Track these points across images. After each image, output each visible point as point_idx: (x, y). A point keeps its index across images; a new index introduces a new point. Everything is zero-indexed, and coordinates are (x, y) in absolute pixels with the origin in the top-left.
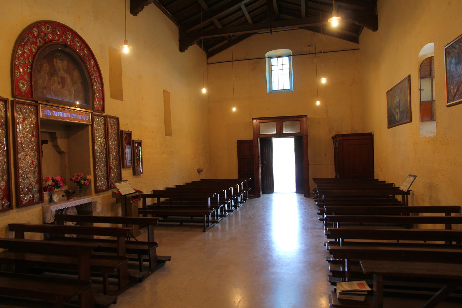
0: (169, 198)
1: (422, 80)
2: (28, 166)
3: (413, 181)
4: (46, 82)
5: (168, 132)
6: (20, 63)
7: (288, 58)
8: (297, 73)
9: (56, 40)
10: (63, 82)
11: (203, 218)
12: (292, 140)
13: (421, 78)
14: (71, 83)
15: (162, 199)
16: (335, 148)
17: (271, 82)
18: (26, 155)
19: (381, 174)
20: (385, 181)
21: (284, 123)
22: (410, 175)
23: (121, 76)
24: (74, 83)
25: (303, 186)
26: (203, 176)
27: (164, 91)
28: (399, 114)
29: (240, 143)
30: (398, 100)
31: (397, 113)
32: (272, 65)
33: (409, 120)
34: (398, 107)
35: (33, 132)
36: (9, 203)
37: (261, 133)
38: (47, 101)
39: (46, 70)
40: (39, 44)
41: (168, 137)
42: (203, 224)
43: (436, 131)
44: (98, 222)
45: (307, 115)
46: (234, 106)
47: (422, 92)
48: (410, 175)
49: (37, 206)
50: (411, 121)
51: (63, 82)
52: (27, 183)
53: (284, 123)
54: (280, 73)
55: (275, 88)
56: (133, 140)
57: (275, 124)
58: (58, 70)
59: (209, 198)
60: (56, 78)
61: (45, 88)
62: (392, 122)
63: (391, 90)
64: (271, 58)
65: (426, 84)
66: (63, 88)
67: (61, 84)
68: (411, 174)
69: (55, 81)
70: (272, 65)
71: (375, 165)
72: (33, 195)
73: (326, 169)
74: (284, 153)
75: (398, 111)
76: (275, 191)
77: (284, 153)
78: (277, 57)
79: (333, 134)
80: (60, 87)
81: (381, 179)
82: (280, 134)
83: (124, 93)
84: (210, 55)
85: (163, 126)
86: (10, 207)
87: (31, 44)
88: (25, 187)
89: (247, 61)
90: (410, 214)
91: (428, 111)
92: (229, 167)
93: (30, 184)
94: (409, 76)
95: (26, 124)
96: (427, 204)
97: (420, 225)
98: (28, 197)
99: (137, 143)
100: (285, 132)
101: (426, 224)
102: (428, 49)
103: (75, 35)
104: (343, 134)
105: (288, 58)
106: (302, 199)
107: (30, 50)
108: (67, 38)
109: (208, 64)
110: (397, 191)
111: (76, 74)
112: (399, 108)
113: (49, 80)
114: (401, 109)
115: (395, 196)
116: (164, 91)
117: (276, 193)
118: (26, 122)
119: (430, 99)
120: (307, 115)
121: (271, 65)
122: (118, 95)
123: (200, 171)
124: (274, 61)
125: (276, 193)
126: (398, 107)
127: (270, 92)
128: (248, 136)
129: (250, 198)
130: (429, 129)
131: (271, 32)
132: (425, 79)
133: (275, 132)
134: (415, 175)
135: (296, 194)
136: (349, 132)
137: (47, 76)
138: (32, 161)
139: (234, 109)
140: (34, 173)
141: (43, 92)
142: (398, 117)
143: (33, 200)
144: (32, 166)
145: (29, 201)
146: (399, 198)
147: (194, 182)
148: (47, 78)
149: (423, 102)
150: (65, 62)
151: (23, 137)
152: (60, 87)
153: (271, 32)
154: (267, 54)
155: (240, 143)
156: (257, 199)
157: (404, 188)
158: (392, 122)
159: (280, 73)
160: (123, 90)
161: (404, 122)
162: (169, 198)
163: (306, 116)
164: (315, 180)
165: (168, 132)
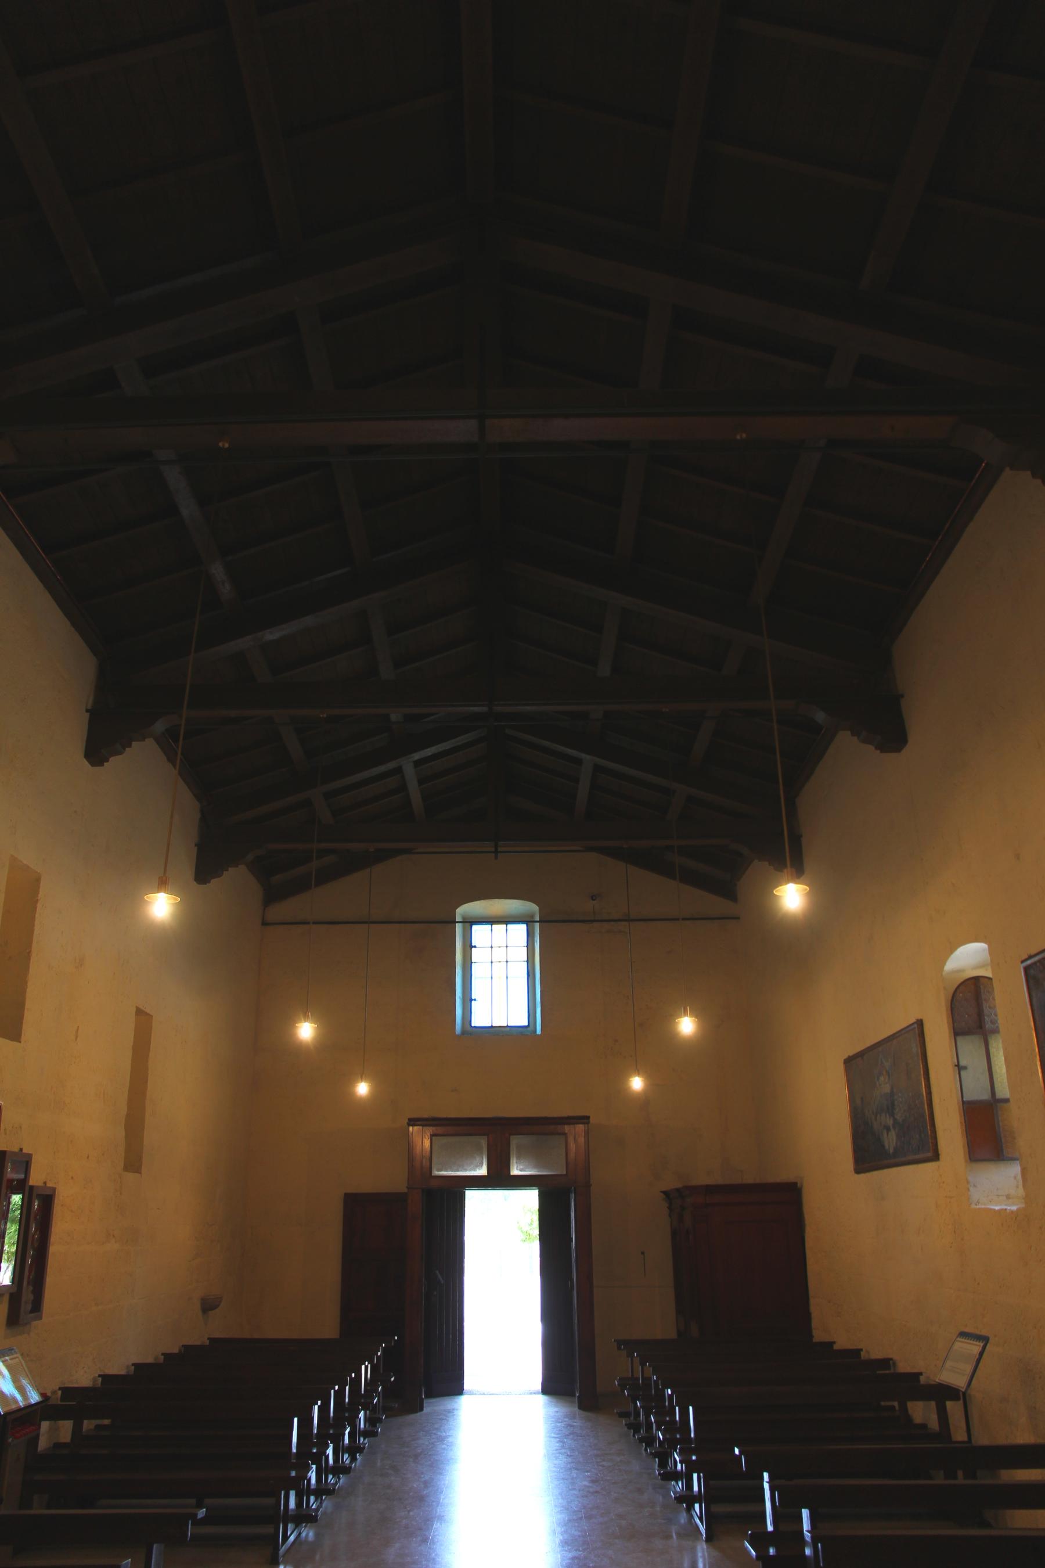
1: (959, 1039)
3: (981, 1354)
5: (133, 1162)
7: (524, 927)
8: (555, 973)
11: (271, 1501)
12: (529, 1199)
13: (958, 1032)
15: (88, 1425)
16: (674, 1233)
17: (468, 1000)
19: (833, 1324)
20: (858, 1351)
21: (515, 1141)
22: (963, 1334)
23: (26, 955)
25: (569, 1372)
26: (221, 1326)
27: (139, 1012)
28: (893, 1134)
29: (355, 1205)
30: (886, 1089)
31: (888, 1130)
32: (471, 947)
33: (930, 1154)
34: (890, 1109)
37: (436, 1173)
41: (131, 1176)
42: (270, 1530)
43: (1021, 1192)
45: (588, 1118)
46: (362, 1077)
47: (963, 1073)
48: (963, 1334)
50: (936, 1157)
53: (515, 1141)
54: (499, 974)
55: (480, 1019)
57: (483, 1142)
59: (296, 1419)
62: (869, 1155)
63: (861, 1054)
64: (470, 922)
65: (970, 1050)
68: (967, 1330)
70: (471, 947)
71: (811, 1293)
73: (644, 1303)
74: (501, 1240)
75: (890, 1122)
76: (467, 1385)
77: (501, 1240)
78: (491, 921)
79: (670, 1183)
81: (842, 1342)
82: (499, 1179)
83: (28, 1017)
84: (272, 895)
85: (122, 1133)
89: (397, 925)
90: (960, 1473)
91: (987, 1132)
92: (306, 1297)
94: (920, 1023)
96: (1024, 1437)
97: (1009, 1513)
99: (39, 1196)
100: (515, 1171)
101: (1032, 1511)
102: (969, 957)
104: (707, 1186)
105: (524, 927)
106: (573, 1417)
109: (264, 923)
110: (912, 1386)
112: (892, 1115)
114: (899, 1117)
115: (910, 1404)
116: (139, 1012)
117: (471, 1393)
119: (986, 1096)
120: (588, 1118)
121: (469, 946)
123: (208, 1306)
124: (480, 933)
125: (471, 1393)
126: (890, 1109)
127: (464, 1032)
128: (389, 1179)
129: (392, 1413)
130: (998, 1188)
131: (496, 852)
132: (968, 1038)
133: (483, 1171)
134: (984, 1332)
135: (542, 1399)
136: (716, 1179)
139: (363, 1089)
142: (890, 1141)
146: (922, 1412)
147: (188, 1350)
149: (969, 1103)
153: (496, 852)
154: (463, 910)
155: (355, 1205)
156: (412, 1416)
157: (954, 1376)
158: (869, 1155)
159: (499, 974)
160: (28, 1004)
161: (911, 1157)
163: (584, 1119)
164: (628, 1345)
165: (133, 1162)
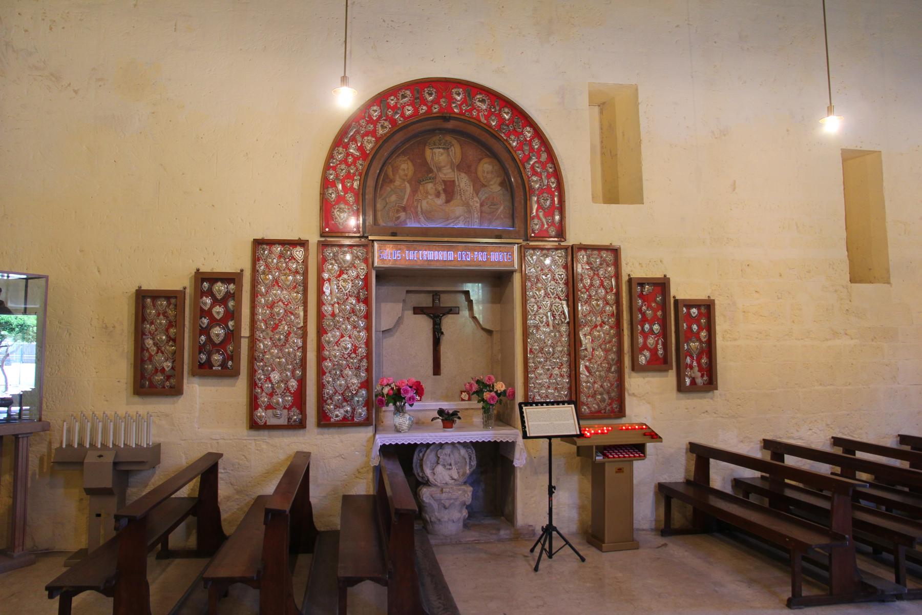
0: (768, 475)
2: (346, 356)
4: (406, 197)
6: (337, 176)
9: (410, 116)
10: (449, 191)
14: (470, 190)
18: (342, 336)
23: (639, 143)
24: (478, 185)
35: (359, 293)
36: (300, 416)
38: (394, 234)
39: (406, 175)
40: (381, 132)
44: (740, 517)
49: (362, 429)
51: (449, 191)
52: (340, 385)
56: (676, 302)
58: (435, 170)
60: (430, 186)
61: (404, 209)
66: (448, 201)
67: (443, 196)
69: (427, 193)
72: (354, 409)
80: (440, 201)
86: (301, 425)
87: (363, 137)
88: (336, 392)
93: (348, 387)
95: (345, 281)
98: (342, 411)
103: (472, 89)
107: (361, 149)
108: (451, 100)
111: (486, 167)
113: (414, 191)
118: (345, 276)
122: (617, 187)
137: (408, 185)
138: (356, 347)
140: (358, 368)
141: (398, 218)
143: (353, 418)
144: (353, 355)
145: (345, 419)
148: (408, 190)
150: (456, 151)
151: (338, 303)
152: (440, 201)
162: (768, 475)
